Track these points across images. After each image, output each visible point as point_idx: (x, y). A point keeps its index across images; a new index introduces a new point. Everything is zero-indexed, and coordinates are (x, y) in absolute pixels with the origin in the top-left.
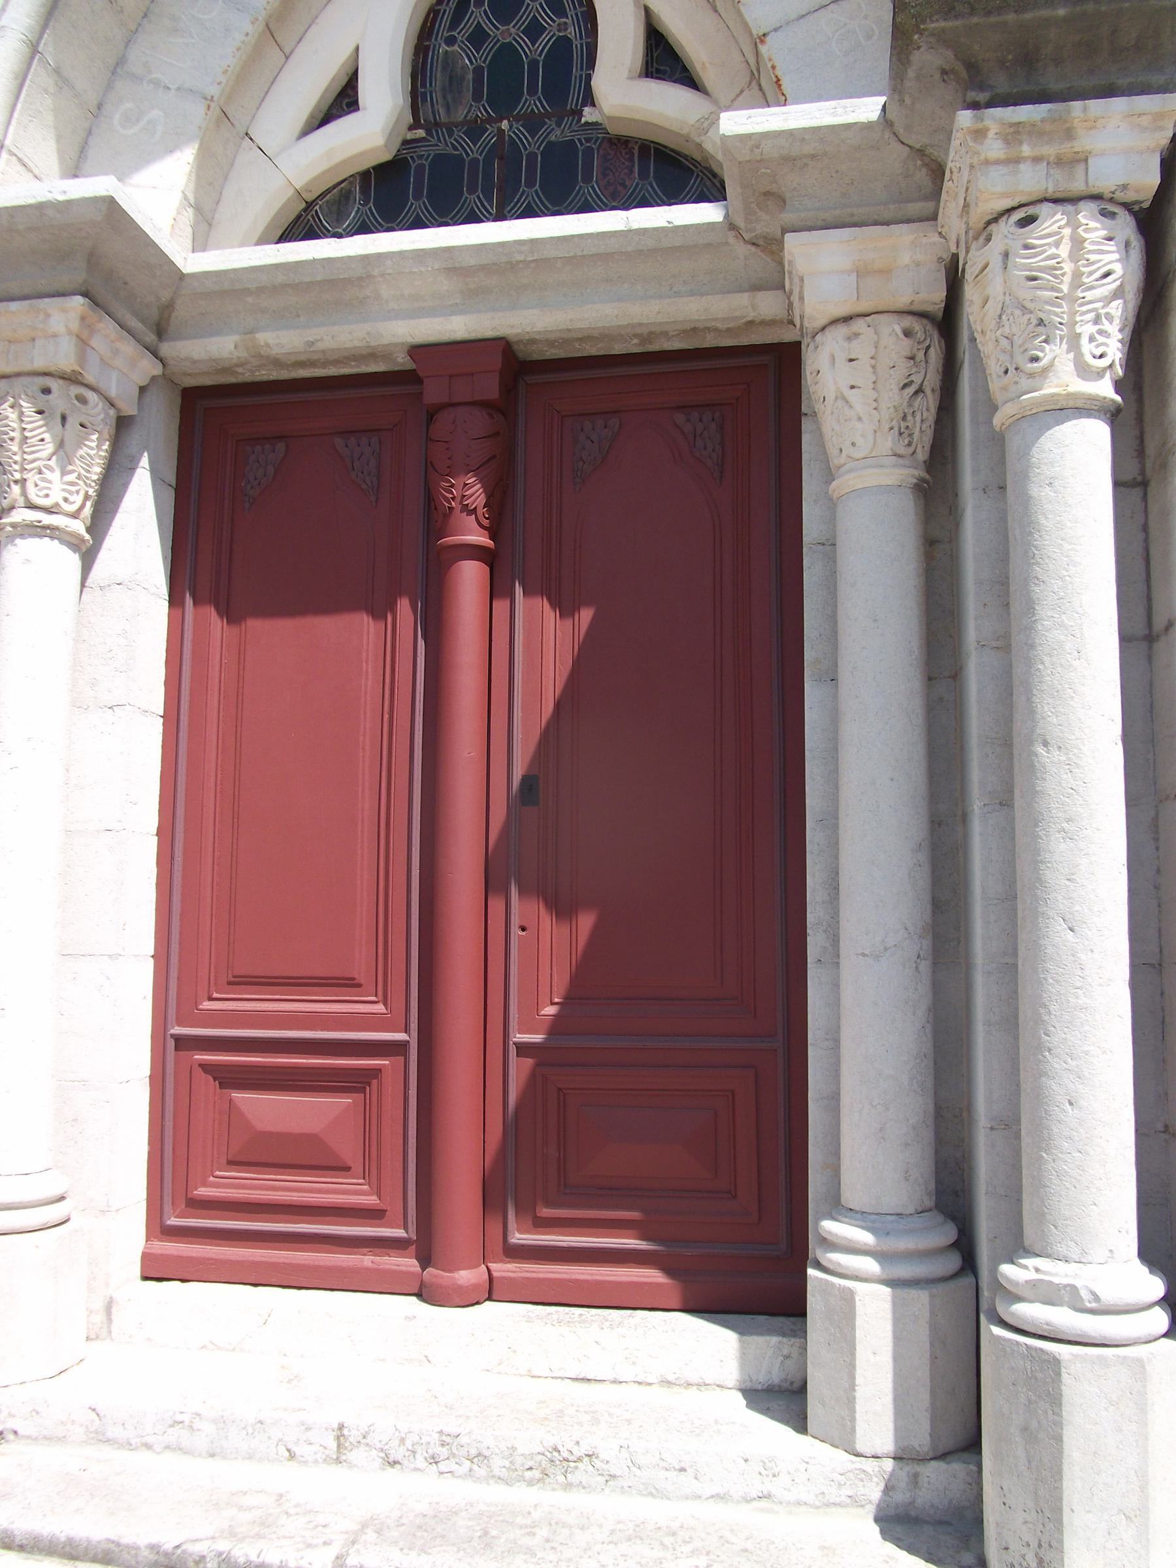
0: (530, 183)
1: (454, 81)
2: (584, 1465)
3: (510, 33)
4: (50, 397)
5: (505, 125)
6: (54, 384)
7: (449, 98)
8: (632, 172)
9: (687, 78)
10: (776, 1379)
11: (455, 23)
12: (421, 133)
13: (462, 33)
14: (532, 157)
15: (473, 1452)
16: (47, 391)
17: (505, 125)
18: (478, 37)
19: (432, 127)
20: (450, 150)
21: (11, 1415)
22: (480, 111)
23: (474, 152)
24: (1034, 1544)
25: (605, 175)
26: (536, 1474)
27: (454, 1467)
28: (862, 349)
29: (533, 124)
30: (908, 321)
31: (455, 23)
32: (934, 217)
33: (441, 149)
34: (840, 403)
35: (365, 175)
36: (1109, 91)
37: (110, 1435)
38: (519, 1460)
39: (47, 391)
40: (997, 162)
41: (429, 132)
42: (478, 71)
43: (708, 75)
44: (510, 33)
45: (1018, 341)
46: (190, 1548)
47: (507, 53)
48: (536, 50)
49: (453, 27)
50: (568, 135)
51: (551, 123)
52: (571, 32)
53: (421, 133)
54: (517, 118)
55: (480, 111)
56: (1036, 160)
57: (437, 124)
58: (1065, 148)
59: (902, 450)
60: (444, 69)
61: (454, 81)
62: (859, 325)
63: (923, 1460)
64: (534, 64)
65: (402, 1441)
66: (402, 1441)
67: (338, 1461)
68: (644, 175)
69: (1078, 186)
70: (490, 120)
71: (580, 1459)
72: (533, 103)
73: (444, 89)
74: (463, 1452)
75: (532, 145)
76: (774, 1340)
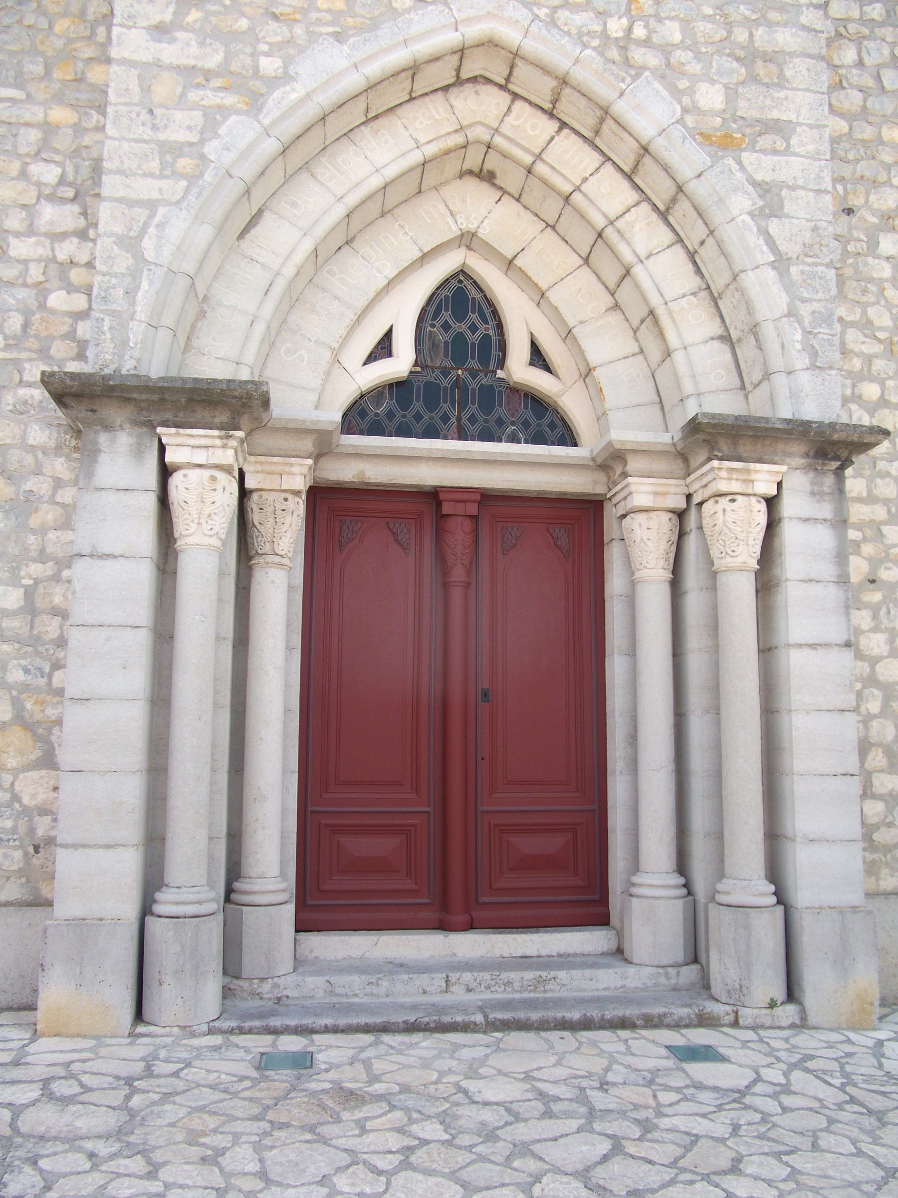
0: (473, 403)
1: (434, 346)
2: (553, 981)
3: (463, 327)
4: (288, 503)
5: (460, 372)
6: (290, 497)
7: (432, 353)
8: (520, 406)
9: (547, 368)
10: (605, 949)
11: (435, 317)
12: (419, 369)
13: (438, 323)
14: (473, 390)
15: (506, 981)
16: (286, 500)
17: (460, 372)
18: (446, 327)
19: (425, 367)
20: (433, 380)
21: (285, 988)
22: (448, 363)
23: (445, 383)
24: (738, 981)
25: (508, 405)
26: (532, 987)
27: (497, 988)
28: (654, 524)
29: (474, 374)
30: (670, 515)
31: (435, 317)
32: (462, 270)
33: (428, 378)
34: (642, 544)
35: (391, 385)
36: (761, 461)
37: (337, 992)
38: (525, 983)
39: (286, 500)
40: (724, 479)
41: (422, 368)
42: (446, 343)
43: (561, 371)
44: (463, 327)
45: (727, 543)
46: (422, 1020)
47: (459, 338)
48: (474, 338)
49: (434, 318)
50: (490, 383)
51: (482, 375)
52: (491, 332)
53: (419, 369)
54: (466, 370)
55: (448, 363)
56: (737, 480)
57: (427, 366)
58: (748, 478)
59: (666, 567)
60: (429, 339)
61: (434, 346)
62: (653, 515)
63: (680, 966)
64: (473, 345)
65: (475, 980)
66: (475, 980)
67: (446, 992)
68: (526, 407)
69: (750, 492)
70: (452, 368)
71: (550, 980)
72: (473, 364)
73: (429, 349)
74: (501, 982)
75: (473, 385)
76: (604, 932)
